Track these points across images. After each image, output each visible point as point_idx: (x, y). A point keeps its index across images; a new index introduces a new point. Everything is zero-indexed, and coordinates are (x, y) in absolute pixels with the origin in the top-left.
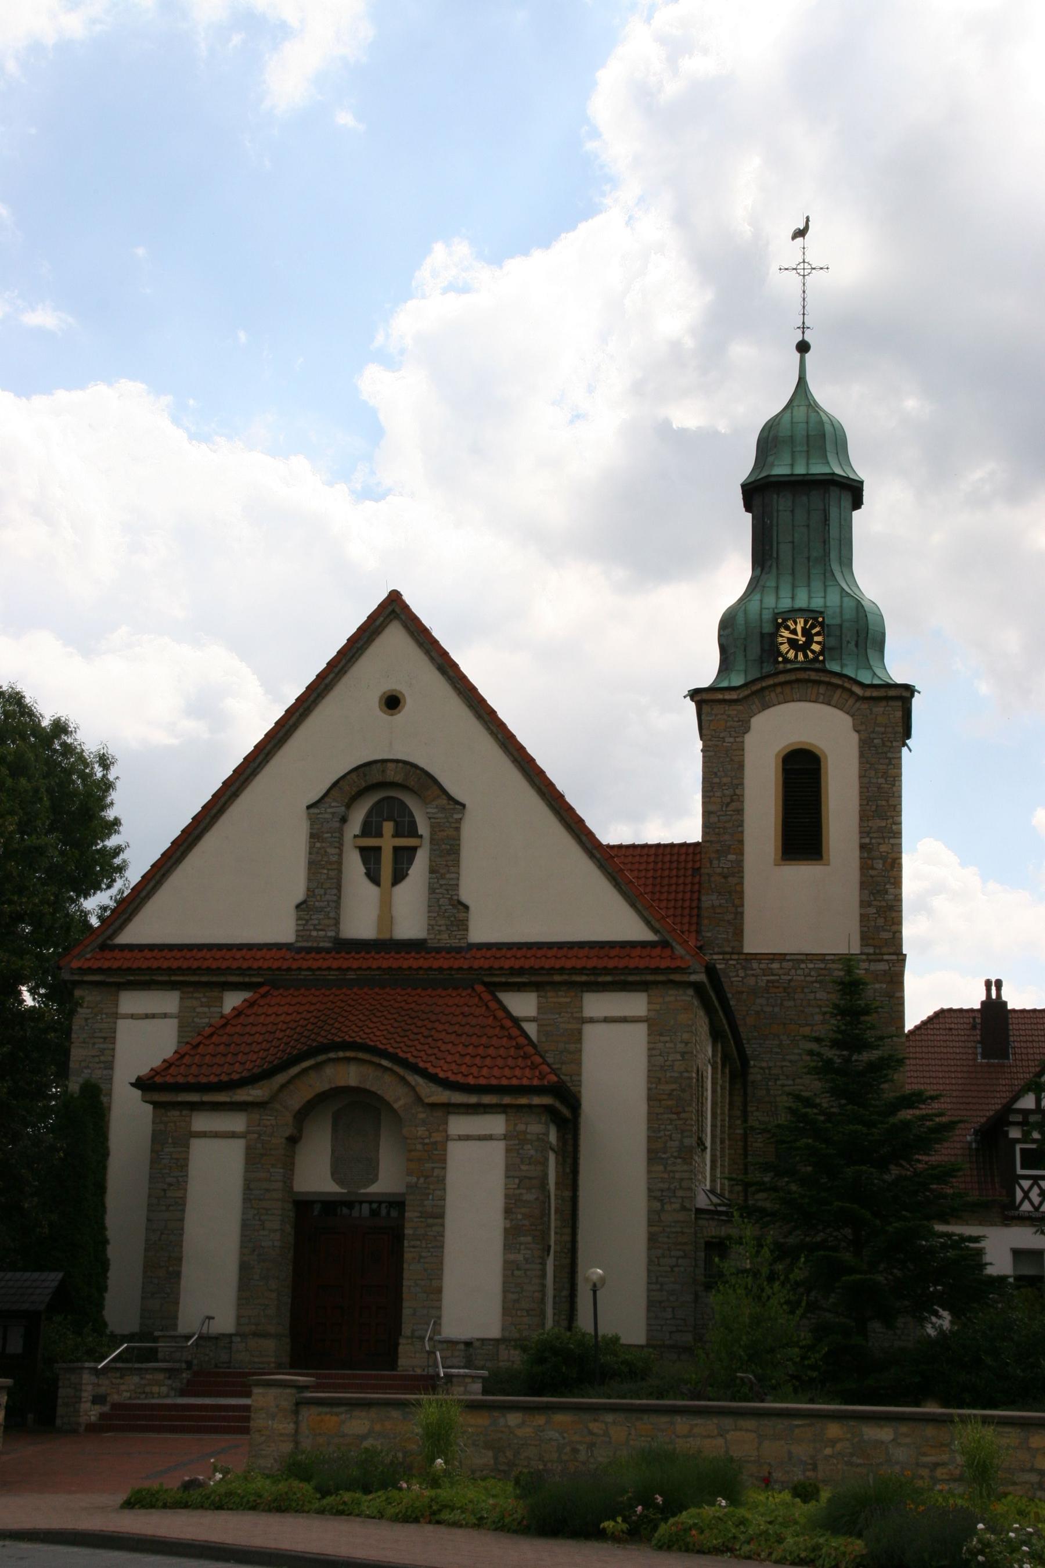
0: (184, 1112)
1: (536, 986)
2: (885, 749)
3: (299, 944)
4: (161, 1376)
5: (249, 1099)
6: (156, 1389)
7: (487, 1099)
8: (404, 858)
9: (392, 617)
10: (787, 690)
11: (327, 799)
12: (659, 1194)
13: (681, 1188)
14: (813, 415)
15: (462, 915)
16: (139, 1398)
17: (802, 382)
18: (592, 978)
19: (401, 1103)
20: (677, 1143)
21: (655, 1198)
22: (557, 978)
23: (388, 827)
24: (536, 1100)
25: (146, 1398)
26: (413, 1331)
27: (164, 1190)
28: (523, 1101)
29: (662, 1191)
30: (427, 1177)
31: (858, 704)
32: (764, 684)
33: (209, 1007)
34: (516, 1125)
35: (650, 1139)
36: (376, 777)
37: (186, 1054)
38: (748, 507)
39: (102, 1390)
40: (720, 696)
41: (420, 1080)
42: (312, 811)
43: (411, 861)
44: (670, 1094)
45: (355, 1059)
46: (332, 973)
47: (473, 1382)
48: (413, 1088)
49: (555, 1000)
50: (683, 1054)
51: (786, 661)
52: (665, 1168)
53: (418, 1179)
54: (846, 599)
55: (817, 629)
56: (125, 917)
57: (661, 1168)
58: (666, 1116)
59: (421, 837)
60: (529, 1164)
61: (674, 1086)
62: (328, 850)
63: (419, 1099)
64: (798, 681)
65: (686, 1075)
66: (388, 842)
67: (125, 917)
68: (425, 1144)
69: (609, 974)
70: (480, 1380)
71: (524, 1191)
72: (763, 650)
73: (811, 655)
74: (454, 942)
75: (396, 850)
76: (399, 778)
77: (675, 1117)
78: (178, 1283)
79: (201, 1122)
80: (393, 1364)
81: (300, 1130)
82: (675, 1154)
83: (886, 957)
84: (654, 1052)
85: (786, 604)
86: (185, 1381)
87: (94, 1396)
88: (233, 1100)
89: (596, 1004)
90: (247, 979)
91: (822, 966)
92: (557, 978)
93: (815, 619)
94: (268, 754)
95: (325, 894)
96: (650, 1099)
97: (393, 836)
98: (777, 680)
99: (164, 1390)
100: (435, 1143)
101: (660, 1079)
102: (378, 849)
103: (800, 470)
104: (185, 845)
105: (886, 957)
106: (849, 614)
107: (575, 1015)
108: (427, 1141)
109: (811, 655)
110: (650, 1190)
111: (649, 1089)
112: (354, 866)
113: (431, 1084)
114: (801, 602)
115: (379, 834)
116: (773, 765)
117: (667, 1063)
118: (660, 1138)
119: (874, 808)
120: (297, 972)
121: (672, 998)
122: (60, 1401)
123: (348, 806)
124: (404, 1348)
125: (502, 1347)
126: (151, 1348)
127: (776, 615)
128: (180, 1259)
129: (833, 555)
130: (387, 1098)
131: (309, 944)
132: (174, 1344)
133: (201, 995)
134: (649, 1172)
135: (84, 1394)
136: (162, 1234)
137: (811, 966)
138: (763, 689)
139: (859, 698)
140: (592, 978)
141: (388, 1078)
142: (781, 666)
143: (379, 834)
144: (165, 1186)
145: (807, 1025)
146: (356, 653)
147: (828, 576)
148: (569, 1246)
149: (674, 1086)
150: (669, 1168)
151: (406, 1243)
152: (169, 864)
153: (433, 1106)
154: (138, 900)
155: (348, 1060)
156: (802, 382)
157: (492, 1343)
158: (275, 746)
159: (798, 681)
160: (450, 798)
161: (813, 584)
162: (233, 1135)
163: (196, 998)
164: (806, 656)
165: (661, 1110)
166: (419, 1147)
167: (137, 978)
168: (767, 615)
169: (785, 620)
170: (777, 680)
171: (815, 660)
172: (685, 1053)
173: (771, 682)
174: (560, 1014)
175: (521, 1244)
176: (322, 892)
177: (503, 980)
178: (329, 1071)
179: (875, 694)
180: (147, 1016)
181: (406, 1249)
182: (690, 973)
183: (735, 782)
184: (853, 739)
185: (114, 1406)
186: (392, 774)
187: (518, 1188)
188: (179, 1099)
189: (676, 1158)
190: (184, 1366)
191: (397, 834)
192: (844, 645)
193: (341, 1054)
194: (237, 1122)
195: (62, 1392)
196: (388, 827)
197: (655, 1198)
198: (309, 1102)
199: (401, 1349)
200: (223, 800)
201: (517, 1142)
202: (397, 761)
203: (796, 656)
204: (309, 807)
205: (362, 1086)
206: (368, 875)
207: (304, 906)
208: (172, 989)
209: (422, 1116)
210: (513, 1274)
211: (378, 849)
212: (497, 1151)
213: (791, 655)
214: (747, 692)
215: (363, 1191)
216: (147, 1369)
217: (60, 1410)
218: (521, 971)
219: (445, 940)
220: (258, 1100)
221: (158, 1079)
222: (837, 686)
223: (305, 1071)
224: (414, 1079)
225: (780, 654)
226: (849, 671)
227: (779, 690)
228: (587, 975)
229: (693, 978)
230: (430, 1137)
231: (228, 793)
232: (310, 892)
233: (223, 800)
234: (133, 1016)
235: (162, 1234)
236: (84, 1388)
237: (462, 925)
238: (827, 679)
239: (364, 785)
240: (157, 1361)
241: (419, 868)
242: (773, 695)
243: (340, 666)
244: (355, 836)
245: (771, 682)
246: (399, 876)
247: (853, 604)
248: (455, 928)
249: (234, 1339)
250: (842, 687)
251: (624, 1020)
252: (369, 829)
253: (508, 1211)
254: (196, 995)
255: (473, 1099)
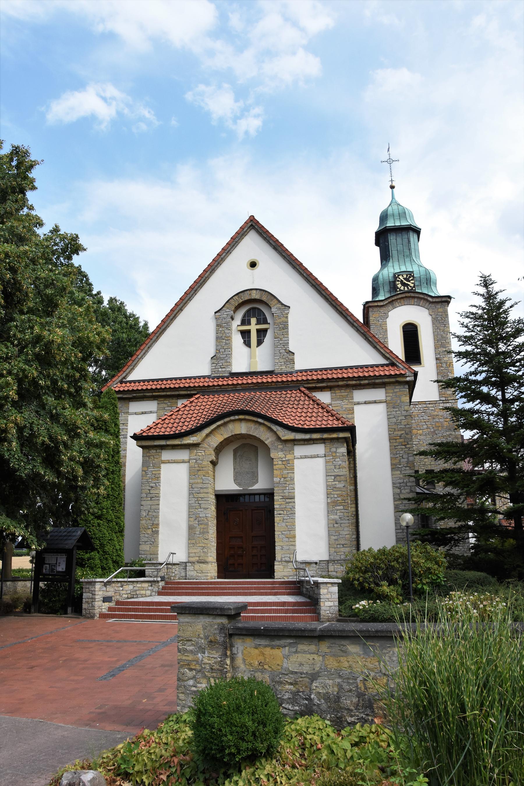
0: (158, 451)
1: (330, 388)
2: (443, 321)
3: (213, 375)
4: (146, 585)
5: (191, 442)
6: (143, 592)
7: (315, 436)
8: (262, 333)
9: (251, 228)
10: (402, 301)
11: (224, 309)
12: (398, 485)
13: (409, 481)
14: (400, 207)
15: (291, 357)
16: (133, 598)
17: (393, 197)
18: (358, 382)
19: (270, 440)
20: (406, 460)
21: (397, 487)
22: (341, 383)
23: (253, 321)
24: (341, 435)
25: (137, 597)
26: (282, 558)
27: (149, 490)
28: (334, 436)
29: (400, 483)
30: (285, 478)
31: (430, 305)
32: (393, 299)
33: (171, 407)
34: (330, 449)
35: (392, 459)
36: (246, 297)
37: (159, 423)
38: (377, 243)
39: (109, 594)
40: (376, 304)
41: (279, 428)
42: (217, 314)
43: (265, 336)
44: (400, 436)
45: (245, 420)
46: (230, 387)
47: (333, 586)
48: (275, 433)
49: (340, 394)
50: (406, 416)
51: (400, 290)
52: (401, 472)
53: (280, 479)
54: (421, 269)
55: (412, 278)
56: (131, 367)
57: (399, 472)
58: (399, 447)
59: (269, 324)
60: (339, 468)
61: (403, 432)
62: (226, 331)
63: (279, 438)
64: (406, 297)
65: (408, 426)
66: (253, 327)
67: (131, 367)
68: (282, 461)
69: (366, 380)
70: (337, 585)
71: (337, 483)
72: (390, 288)
73: (410, 288)
74: (289, 370)
75: (258, 331)
76: (257, 297)
77: (404, 447)
78: (158, 537)
79: (166, 455)
80: (271, 575)
81: (217, 458)
82: (405, 465)
83: (450, 401)
84: (391, 416)
85: (397, 270)
86: (161, 587)
87: (104, 598)
88: (182, 443)
89: (359, 395)
90: (189, 392)
91: (425, 406)
92: (341, 383)
93: (411, 274)
94: (196, 291)
95: (225, 351)
96: (390, 439)
97: (256, 324)
98: (398, 297)
99: (148, 592)
100: (289, 460)
101: (395, 429)
102: (249, 332)
103: (398, 224)
104: (159, 333)
105: (450, 401)
106: (423, 272)
107: (350, 401)
108: (284, 459)
109: (410, 288)
110: (393, 483)
111: (389, 434)
112: (237, 340)
113: (285, 430)
114: (403, 269)
115: (249, 324)
116: (399, 329)
117: (398, 421)
118: (397, 457)
119: (440, 344)
120: (213, 388)
121: (398, 390)
122: (84, 600)
123: (235, 312)
124: (278, 567)
125: (330, 564)
126: (141, 570)
127: (394, 275)
128: (158, 524)
129: (413, 254)
130: (262, 438)
131: (218, 375)
132: (153, 568)
133: (167, 402)
134: (392, 475)
135: (97, 597)
136: (149, 512)
137: (420, 406)
138: (393, 301)
139: (431, 303)
140: (358, 382)
141: (262, 429)
142: (399, 292)
143: (249, 324)
144: (150, 488)
145: (420, 430)
146: (235, 244)
147: (412, 261)
148: (354, 513)
149: (403, 432)
150: (403, 472)
151: (276, 512)
152: (151, 342)
153: (286, 441)
154: (137, 360)
155: (240, 420)
156: (393, 197)
157: (325, 562)
158: (199, 287)
159: (406, 297)
160: (282, 304)
161: (407, 264)
162: (183, 462)
163: (165, 403)
164: (408, 288)
165: (397, 444)
166: (280, 463)
167: (137, 395)
168: (391, 275)
169: (399, 275)
170: (398, 297)
171: (412, 289)
172: (406, 416)
173: (395, 298)
174: (342, 400)
175: (337, 510)
176: (223, 350)
177: (314, 385)
178: (231, 426)
179: (437, 300)
180: (143, 413)
181: (275, 516)
182: (407, 377)
183: (385, 336)
184: (429, 319)
185: (118, 603)
186: (255, 295)
187: (334, 481)
188: (155, 444)
189: (406, 467)
190: (159, 579)
191: (258, 323)
192: (422, 284)
193: (237, 417)
194: (184, 455)
195: (85, 595)
196: (253, 321)
197: (397, 487)
198: (221, 443)
199: (276, 567)
200: (176, 312)
201: (332, 457)
202: (256, 289)
203: (404, 289)
204: (215, 313)
205: (248, 433)
206: (245, 342)
207: (215, 357)
208: (154, 400)
209: (280, 447)
210: (334, 527)
211: (249, 332)
212: (320, 463)
213: (402, 288)
214: (387, 302)
215: (250, 488)
216: (137, 582)
217: (84, 606)
218: (323, 380)
219: (284, 369)
220: (195, 442)
221: (144, 434)
222: (421, 298)
223: (219, 426)
224: (275, 428)
225: (398, 288)
226: (425, 292)
227: (399, 301)
228: (355, 380)
229: (408, 379)
230: (285, 457)
231: (178, 309)
232: (218, 351)
233: (176, 312)
234: (136, 414)
235: (149, 512)
236: (97, 593)
237: (293, 361)
238: (418, 296)
239: (241, 301)
240: (144, 576)
241: (268, 339)
242: (397, 303)
243: (228, 250)
244: (238, 326)
245: (395, 298)
246: (260, 343)
247: (424, 269)
248: (288, 363)
249: (188, 564)
250: (424, 299)
251: (375, 402)
252: (245, 321)
253: (328, 495)
254: (165, 402)
255: (307, 436)
